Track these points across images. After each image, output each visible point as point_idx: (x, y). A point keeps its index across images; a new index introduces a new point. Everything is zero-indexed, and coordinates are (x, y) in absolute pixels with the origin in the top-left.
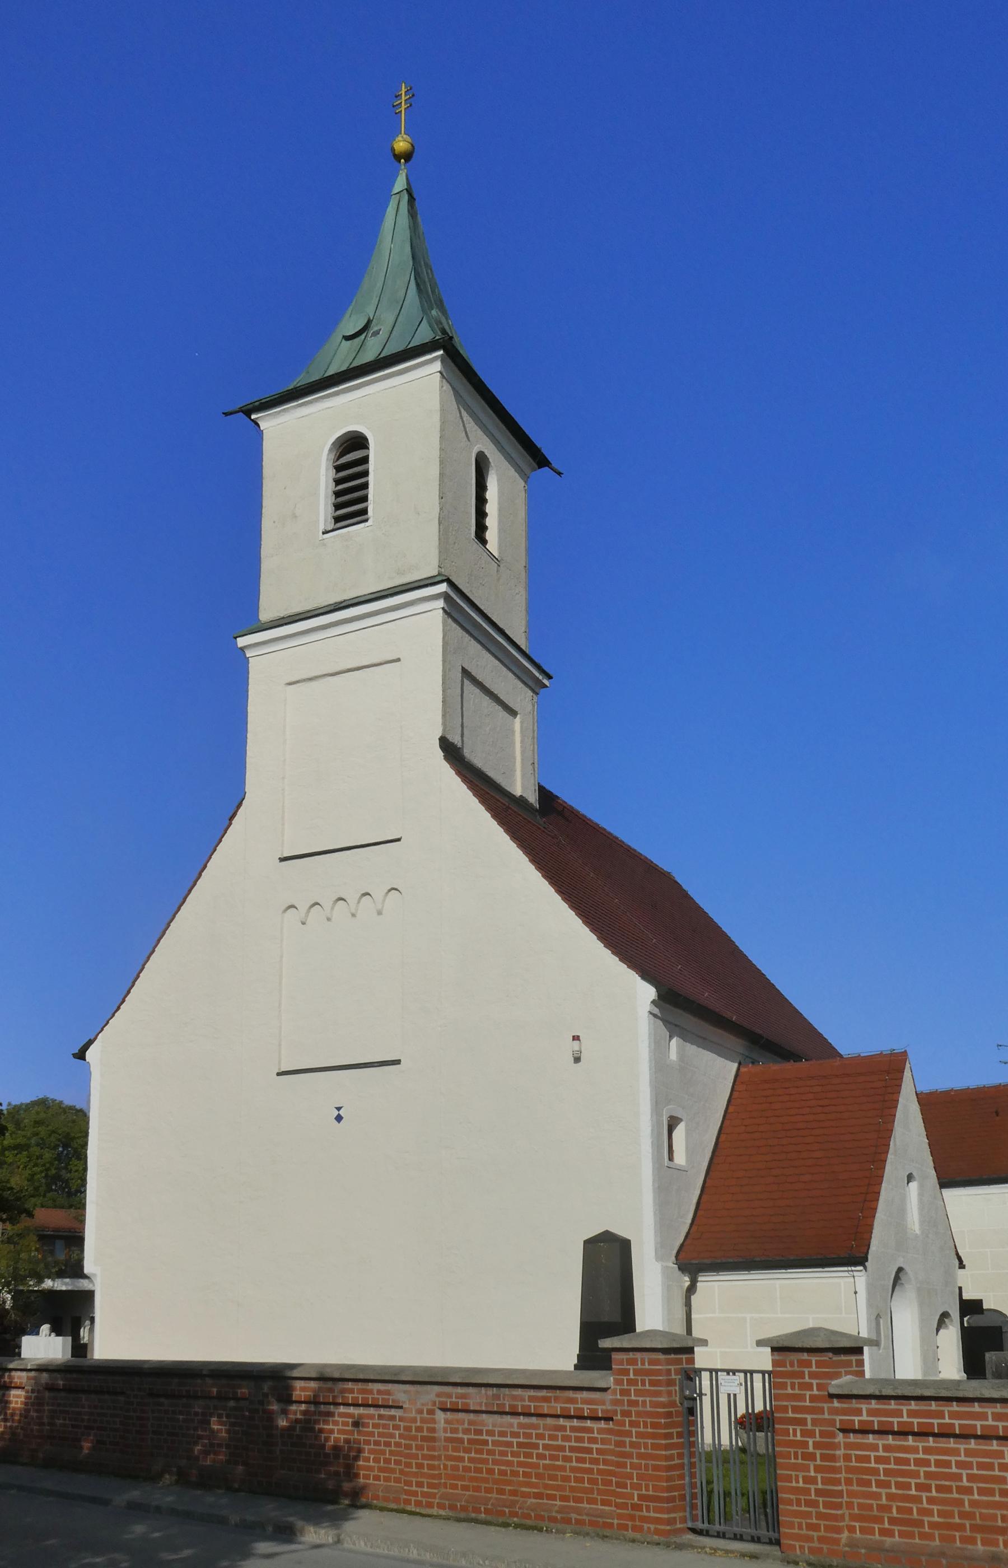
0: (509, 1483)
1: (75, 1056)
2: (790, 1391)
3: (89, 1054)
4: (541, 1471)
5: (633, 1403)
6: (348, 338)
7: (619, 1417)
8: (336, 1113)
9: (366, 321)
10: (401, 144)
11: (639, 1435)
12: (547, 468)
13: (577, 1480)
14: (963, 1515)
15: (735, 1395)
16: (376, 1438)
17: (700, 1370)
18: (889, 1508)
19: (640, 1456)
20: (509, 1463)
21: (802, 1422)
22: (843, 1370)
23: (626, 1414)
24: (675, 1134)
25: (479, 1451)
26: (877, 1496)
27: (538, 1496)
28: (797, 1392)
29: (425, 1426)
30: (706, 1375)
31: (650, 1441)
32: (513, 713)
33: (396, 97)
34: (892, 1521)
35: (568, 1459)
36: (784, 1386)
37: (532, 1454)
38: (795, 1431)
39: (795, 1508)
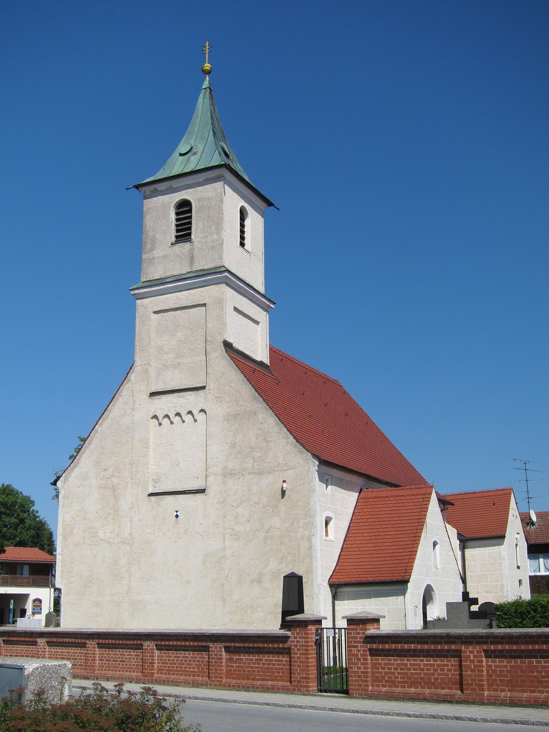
0: (252, 675)
1: (52, 484)
2: (353, 635)
3: (59, 483)
4: (264, 670)
5: (298, 642)
6: (181, 155)
7: (293, 647)
8: (176, 513)
9: (190, 148)
10: (207, 66)
11: (301, 654)
12: (272, 207)
13: (278, 672)
14: (408, 678)
15: (329, 637)
16: (198, 659)
17: (323, 628)
18: (385, 677)
19: (301, 662)
20: (251, 667)
21: (357, 647)
22: (371, 627)
23: (296, 646)
24: (329, 527)
25: (240, 663)
26: (381, 673)
27: (263, 680)
28: (355, 635)
29: (218, 653)
30: (325, 630)
31: (304, 656)
32: (257, 323)
33: (204, 46)
34: (386, 681)
35: (274, 665)
36: (350, 633)
37: (260, 663)
38: (354, 650)
39: (354, 678)
